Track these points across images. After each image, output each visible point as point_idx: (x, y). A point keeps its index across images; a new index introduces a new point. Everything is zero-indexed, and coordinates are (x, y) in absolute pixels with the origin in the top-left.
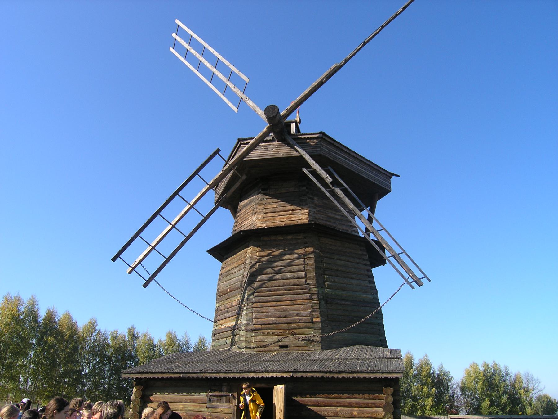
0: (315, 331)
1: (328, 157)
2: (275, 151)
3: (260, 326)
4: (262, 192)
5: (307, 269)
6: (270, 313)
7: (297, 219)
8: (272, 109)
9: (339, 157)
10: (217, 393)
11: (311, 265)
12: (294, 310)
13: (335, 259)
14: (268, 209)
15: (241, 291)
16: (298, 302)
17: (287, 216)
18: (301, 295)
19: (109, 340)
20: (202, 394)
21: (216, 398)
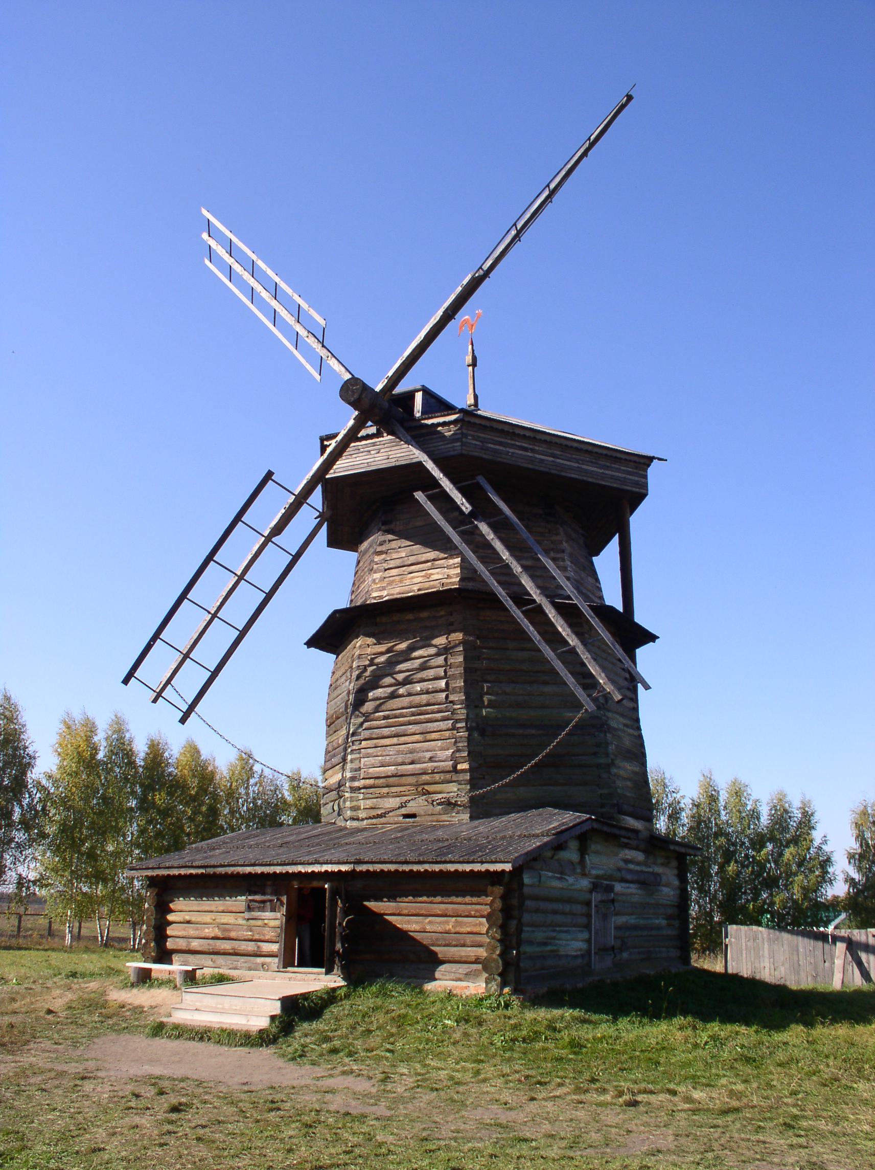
0: (460, 787)
1: (481, 455)
2: (384, 454)
3: (371, 782)
4: (383, 527)
5: (451, 673)
6: (388, 758)
7: (440, 577)
8: (351, 385)
9: (508, 449)
10: (258, 897)
11: (458, 667)
12: (427, 751)
13: (508, 649)
14: (392, 562)
15: (347, 718)
16: (434, 736)
17: (423, 573)
18: (438, 723)
19: (286, 794)
20: (239, 898)
21: (257, 904)
